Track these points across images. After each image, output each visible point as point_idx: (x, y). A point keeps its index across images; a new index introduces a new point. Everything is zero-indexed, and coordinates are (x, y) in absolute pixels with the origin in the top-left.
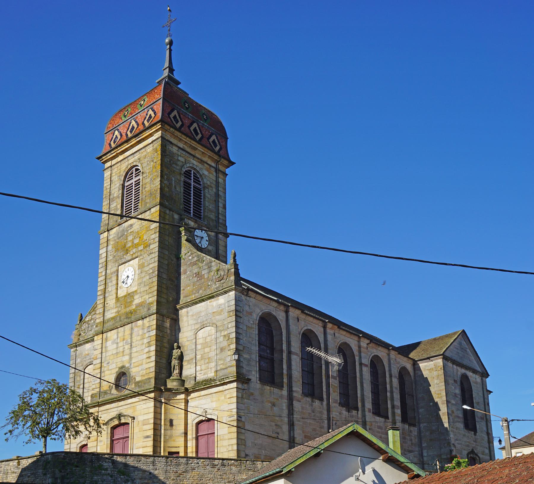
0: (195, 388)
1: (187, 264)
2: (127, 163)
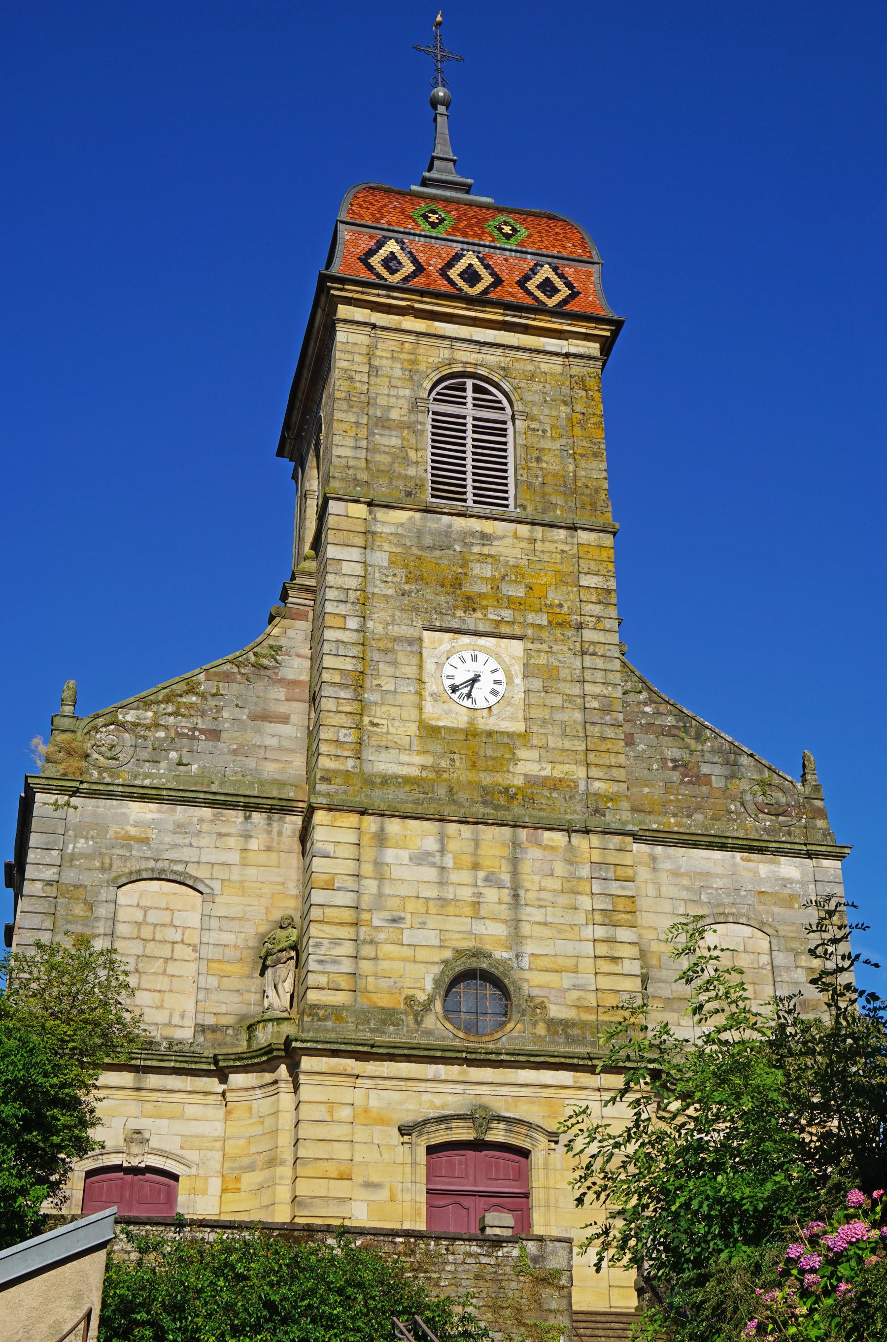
0: (132, 1059)
1: (633, 722)
2: (446, 354)
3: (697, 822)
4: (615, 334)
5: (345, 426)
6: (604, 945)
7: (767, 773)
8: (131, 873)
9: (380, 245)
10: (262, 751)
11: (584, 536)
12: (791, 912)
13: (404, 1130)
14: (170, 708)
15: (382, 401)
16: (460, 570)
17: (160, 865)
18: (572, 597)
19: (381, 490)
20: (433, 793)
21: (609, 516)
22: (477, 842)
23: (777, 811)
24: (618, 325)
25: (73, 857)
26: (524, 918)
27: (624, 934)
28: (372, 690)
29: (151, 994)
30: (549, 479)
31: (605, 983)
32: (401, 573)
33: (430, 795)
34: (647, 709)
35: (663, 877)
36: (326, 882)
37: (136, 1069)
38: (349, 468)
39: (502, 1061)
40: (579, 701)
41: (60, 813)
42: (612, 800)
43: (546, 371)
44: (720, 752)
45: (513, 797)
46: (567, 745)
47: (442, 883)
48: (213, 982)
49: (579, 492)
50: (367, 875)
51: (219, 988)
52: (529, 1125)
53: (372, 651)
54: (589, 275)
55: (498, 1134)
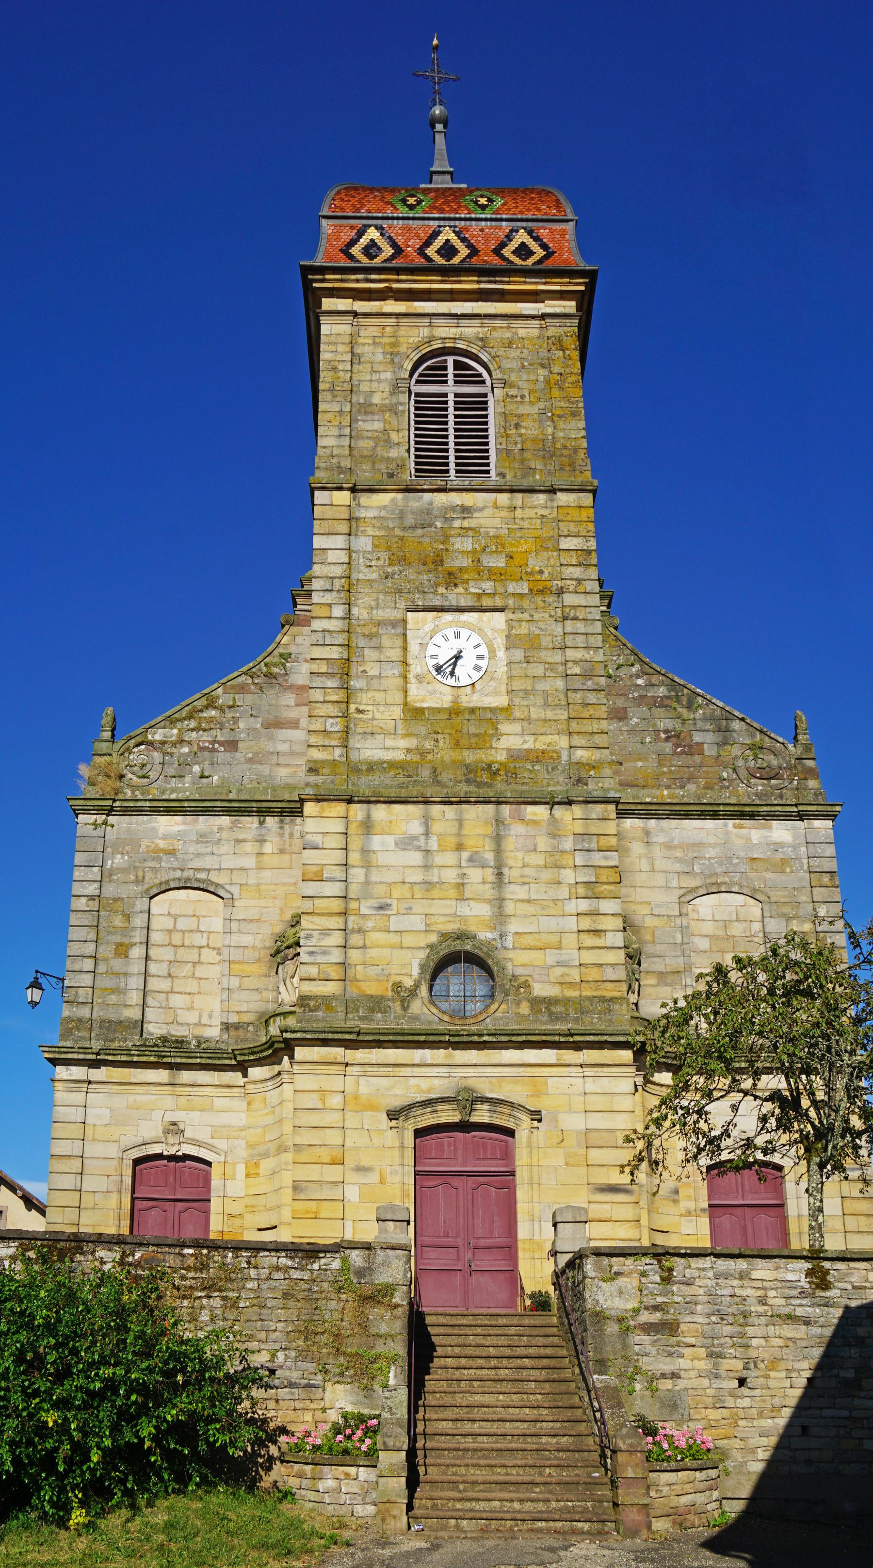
0: (164, 1057)
1: (626, 695)
2: (425, 332)
3: (690, 792)
4: (591, 287)
5: (329, 416)
6: (587, 918)
7: (758, 736)
8: (161, 884)
9: (361, 233)
10: (275, 757)
11: (563, 498)
12: (783, 877)
13: (393, 1115)
14: (193, 724)
15: (364, 387)
16: (442, 547)
17: (186, 874)
18: (552, 562)
19: (365, 475)
20: (417, 775)
21: (588, 474)
22: (460, 822)
23: (768, 775)
24: (592, 275)
25: (111, 873)
26: (508, 896)
27: (608, 906)
28: (358, 677)
29: (183, 996)
30: (528, 445)
31: (588, 957)
32: (384, 555)
33: (415, 778)
34: (640, 682)
35: (657, 851)
36: (315, 873)
37: (170, 1066)
38: (333, 456)
39: (485, 1042)
40: (561, 668)
41: (99, 832)
42: (594, 767)
43: (524, 336)
44: (711, 718)
45: (496, 773)
46: (550, 714)
47: (427, 867)
48: (235, 982)
49: (558, 453)
50: (355, 864)
51: (240, 988)
52: (511, 1105)
53: (357, 638)
54: (563, 233)
55: (482, 1115)
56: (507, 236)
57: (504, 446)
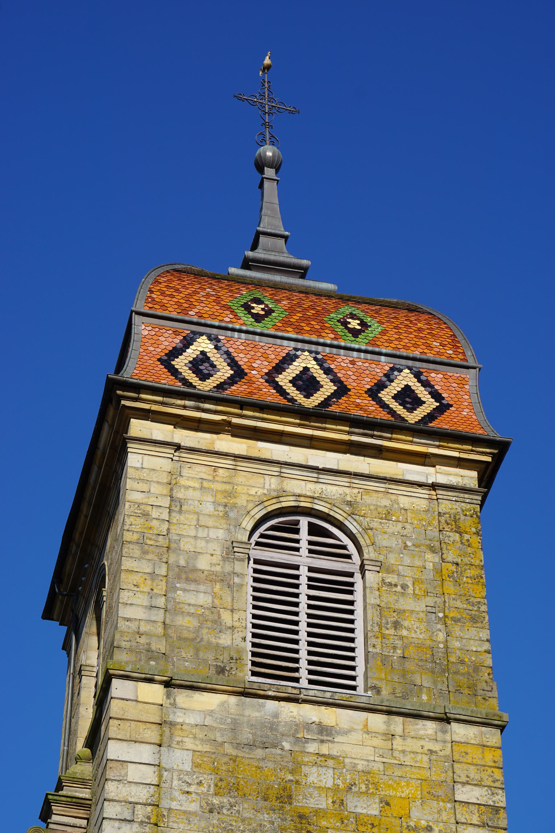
2: (273, 483)
4: (498, 459)
5: (136, 578)
9: (188, 342)
15: (187, 545)
16: (290, 777)
18: (444, 816)
21: (494, 703)
30: (411, 652)
32: (208, 780)
38: (140, 634)
54: (462, 382)
56: (386, 375)
57: (378, 650)
